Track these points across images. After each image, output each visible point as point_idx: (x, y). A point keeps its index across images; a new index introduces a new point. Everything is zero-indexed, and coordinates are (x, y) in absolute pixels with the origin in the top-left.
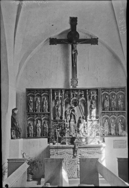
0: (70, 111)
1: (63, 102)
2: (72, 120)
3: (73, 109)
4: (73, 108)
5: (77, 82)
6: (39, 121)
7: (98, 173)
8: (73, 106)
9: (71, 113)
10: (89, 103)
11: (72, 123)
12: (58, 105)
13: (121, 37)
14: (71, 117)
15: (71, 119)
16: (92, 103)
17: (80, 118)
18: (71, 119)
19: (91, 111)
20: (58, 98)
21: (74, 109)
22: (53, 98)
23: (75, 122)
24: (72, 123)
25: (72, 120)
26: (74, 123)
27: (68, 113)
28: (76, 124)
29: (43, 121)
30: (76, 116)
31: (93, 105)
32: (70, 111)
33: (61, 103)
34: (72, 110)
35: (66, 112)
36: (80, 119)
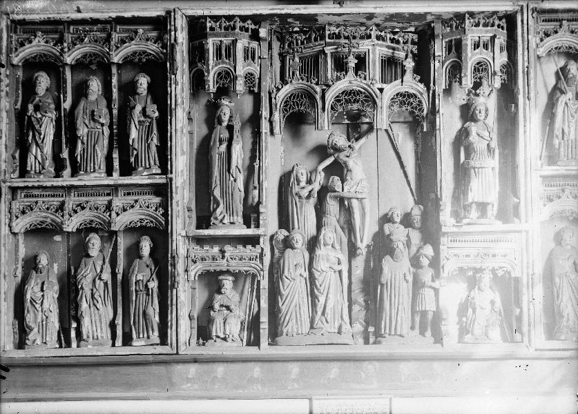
0: (314, 171)
1: (265, 113)
2: (332, 233)
3: (336, 162)
4: (338, 150)
5: (10, 227)
6: (95, 242)
7: (476, 285)
8: (341, 141)
9: (324, 191)
10: (448, 121)
11: (331, 256)
12: (230, 128)
13: (63, 355)
14: (320, 211)
15: (319, 226)
16: (468, 113)
17: (386, 219)
18: (319, 226)
19: (462, 173)
20: (227, 78)
21: (342, 156)
22: (198, 82)
23: (352, 251)
24: (331, 256)
25: (332, 233)
26: (344, 258)
27: (301, 188)
28: (359, 263)
29: (123, 243)
30: (355, 203)
31: (474, 128)
32: (314, 171)
33: (254, 121)
34: (326, 170)
35: (285, 183)
36: (387, 228)
